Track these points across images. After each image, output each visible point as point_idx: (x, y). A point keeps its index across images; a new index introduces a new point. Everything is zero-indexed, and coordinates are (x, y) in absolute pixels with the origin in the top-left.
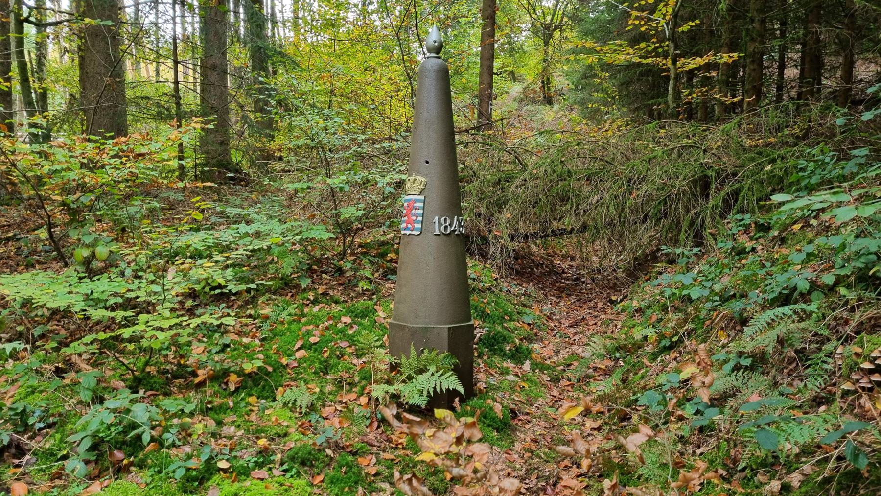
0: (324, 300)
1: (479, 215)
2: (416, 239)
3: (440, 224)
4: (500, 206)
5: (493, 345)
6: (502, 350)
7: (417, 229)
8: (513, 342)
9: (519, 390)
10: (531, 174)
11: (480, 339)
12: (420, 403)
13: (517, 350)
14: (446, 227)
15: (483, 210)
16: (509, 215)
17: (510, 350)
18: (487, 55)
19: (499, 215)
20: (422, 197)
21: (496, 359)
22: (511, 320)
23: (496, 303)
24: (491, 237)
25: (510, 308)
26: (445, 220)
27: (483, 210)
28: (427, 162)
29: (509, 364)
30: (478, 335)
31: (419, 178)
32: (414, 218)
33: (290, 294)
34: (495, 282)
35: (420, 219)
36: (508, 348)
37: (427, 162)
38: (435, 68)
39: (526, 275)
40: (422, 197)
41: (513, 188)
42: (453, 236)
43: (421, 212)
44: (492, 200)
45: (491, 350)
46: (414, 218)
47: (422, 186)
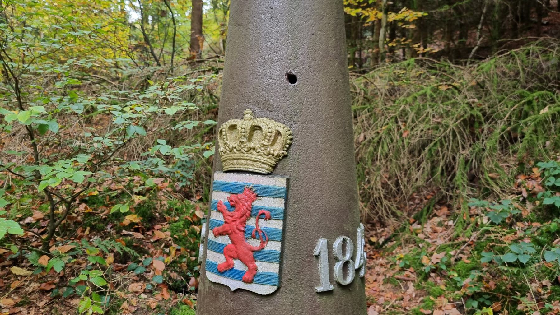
2: (267, 307)
3: (333, 259)
7: (265, 279)
20: (279, 182)
32: (255, 244)
43: (277, 225)
46: (255, 244)
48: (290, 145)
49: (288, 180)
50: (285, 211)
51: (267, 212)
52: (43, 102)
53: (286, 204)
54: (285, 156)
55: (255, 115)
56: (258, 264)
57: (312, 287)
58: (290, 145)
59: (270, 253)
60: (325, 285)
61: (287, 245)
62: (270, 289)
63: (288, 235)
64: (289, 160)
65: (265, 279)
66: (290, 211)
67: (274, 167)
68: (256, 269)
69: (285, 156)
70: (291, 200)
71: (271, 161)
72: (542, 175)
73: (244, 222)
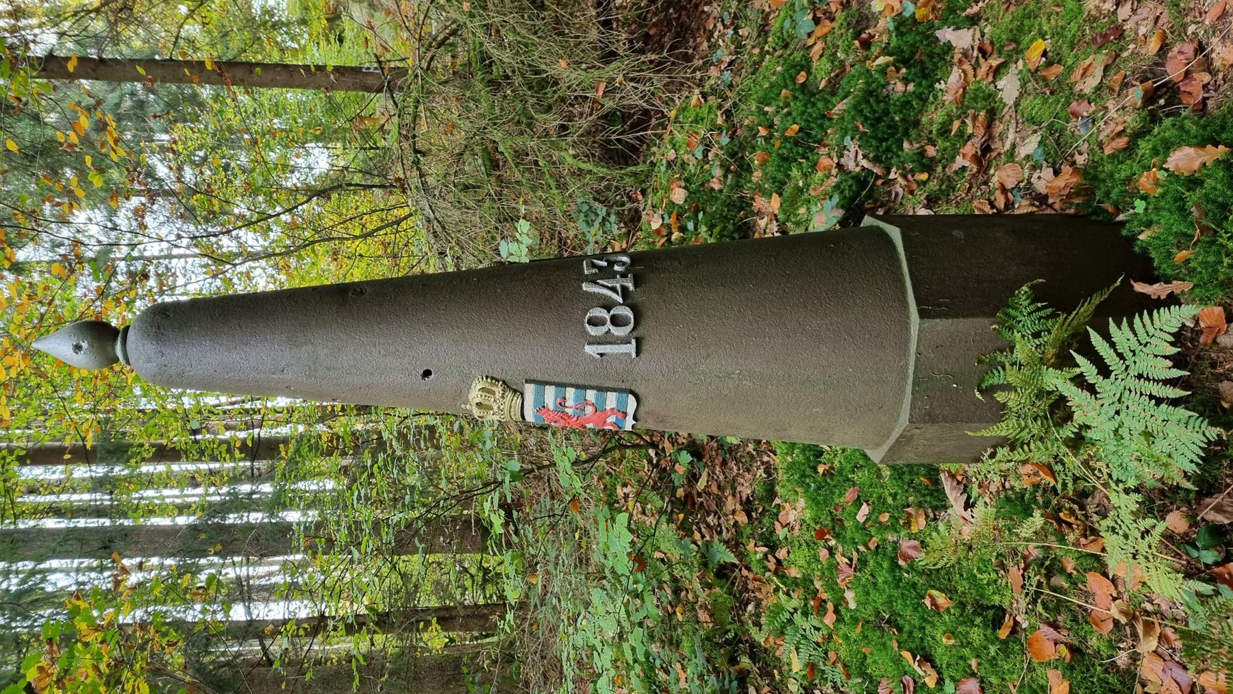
0: (766, 521)
1: (563, 128)
2: (649, 403)
3: (607, 340)
4: (543, 84)
5: (892, 126)
6: (906, 104)
7: (622, 405)
8: (883, 70)
9: (1058, 69)
10: (472, 16)
11: (876, 160)
12: (1199, 439)
13: (906, 62)
14: (616, 321)
15: (552, 121)
16: (563, 63)
17: (906, 81)
18: (284, 77)
19: (563, 86)
20: (530, 390)
21: (933, 117)
22: (806, 65)
23: (765, 101)
24: (609, 104)
25: (773, 68)
26: (594, 322)
27: (552, 121)
28: (427, 373)
29: (951, 83)
30: (865, 163)
31: (475, 395)
32: (589, 410)
33: (745, 572)
34: (713, 101)
35: (591, 395)
36: (900, 87)
37: (427, 373)
38: (150, 348)
39: (684, 18)
40: (530, 390)
41: (507, 56)
42: (640, 298)
43: (570, 393)
44: (532, 101)
45: (906, 134)
46: (589, 410)
47: (498, 390)
48: (492, 378)
49: (527, 381)
50: (557, 385)
51: (559, 401)
52: (1094, 581)
53: (550, 384)
54: (504, 382)
55: (466, 402)
56: (608, 408)
57: (632, 360)
58: (492, 378)
59: (597, 399)
60: (631, 348)
61: (590, 383)
62: (632, 403)
63: (580, 382)
64: (508, 379)
65: (622, 405)
66: (557, 380)
67: (515, 391)
68: (612, 409)
69: (504, 382)
70: (547, 378)
71: (509, 395)
72: (438, 503)
73: (569, 417)
